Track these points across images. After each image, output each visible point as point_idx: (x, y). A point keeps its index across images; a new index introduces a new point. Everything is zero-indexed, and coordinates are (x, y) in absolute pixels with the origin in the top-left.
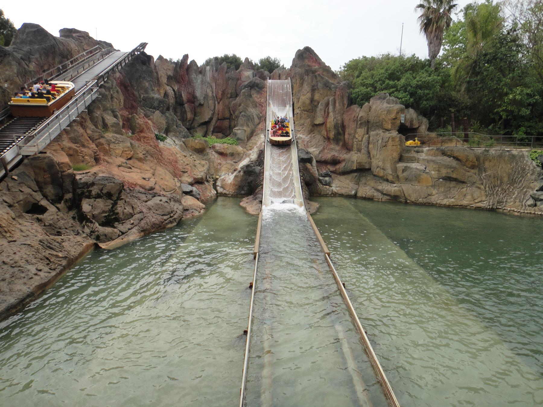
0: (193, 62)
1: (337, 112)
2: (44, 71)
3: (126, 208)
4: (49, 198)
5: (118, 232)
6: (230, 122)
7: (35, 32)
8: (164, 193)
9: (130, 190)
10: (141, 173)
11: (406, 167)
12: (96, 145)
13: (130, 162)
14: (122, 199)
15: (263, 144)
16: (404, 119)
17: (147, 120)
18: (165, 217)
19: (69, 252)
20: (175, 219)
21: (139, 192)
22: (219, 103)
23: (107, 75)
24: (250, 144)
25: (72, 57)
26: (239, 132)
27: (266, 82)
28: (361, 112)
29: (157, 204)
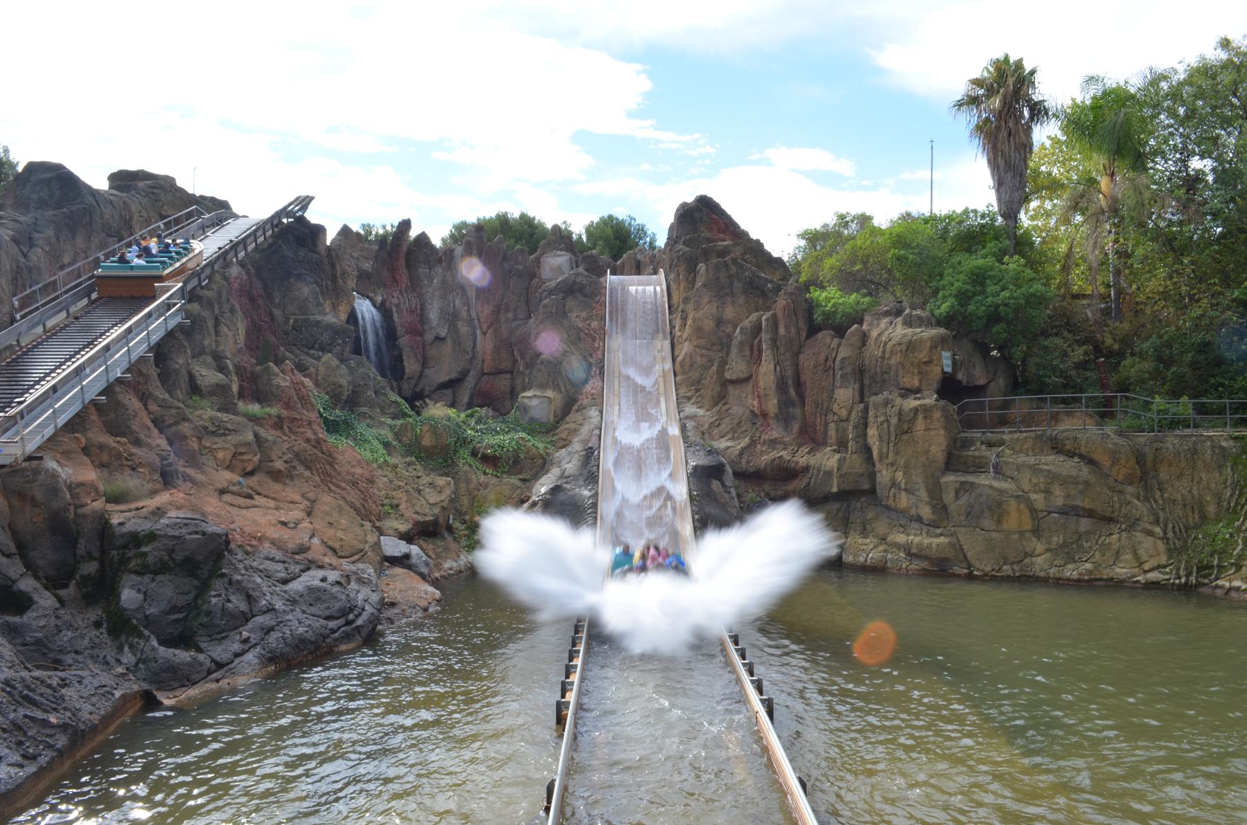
0: (423, 239)
1: (782, 350)
2: (62, 267)
3: (232, 598)
4: (41, 574)
5: (208, 662)
6: (513, 379)
7: (50, 180)
8: (334, 561)
9: (247, 553)
10: (277, 509)
11: (963, 483)
12: (167, 438)
13: (253, 481)
14: (223, 575)
15: (597, 432)
16: (949, 362)
17: (300, 377)
18: (332, 624)
19: (75, 712)
20: (358, 628)
21: (267, 558)
22: (485, 334)
23: (208, 271)
24: (562, 431)
25: (131, 234)
26: (535, 402)
27: (602, 280)
28: (841, 348)
29: (311, 590)
